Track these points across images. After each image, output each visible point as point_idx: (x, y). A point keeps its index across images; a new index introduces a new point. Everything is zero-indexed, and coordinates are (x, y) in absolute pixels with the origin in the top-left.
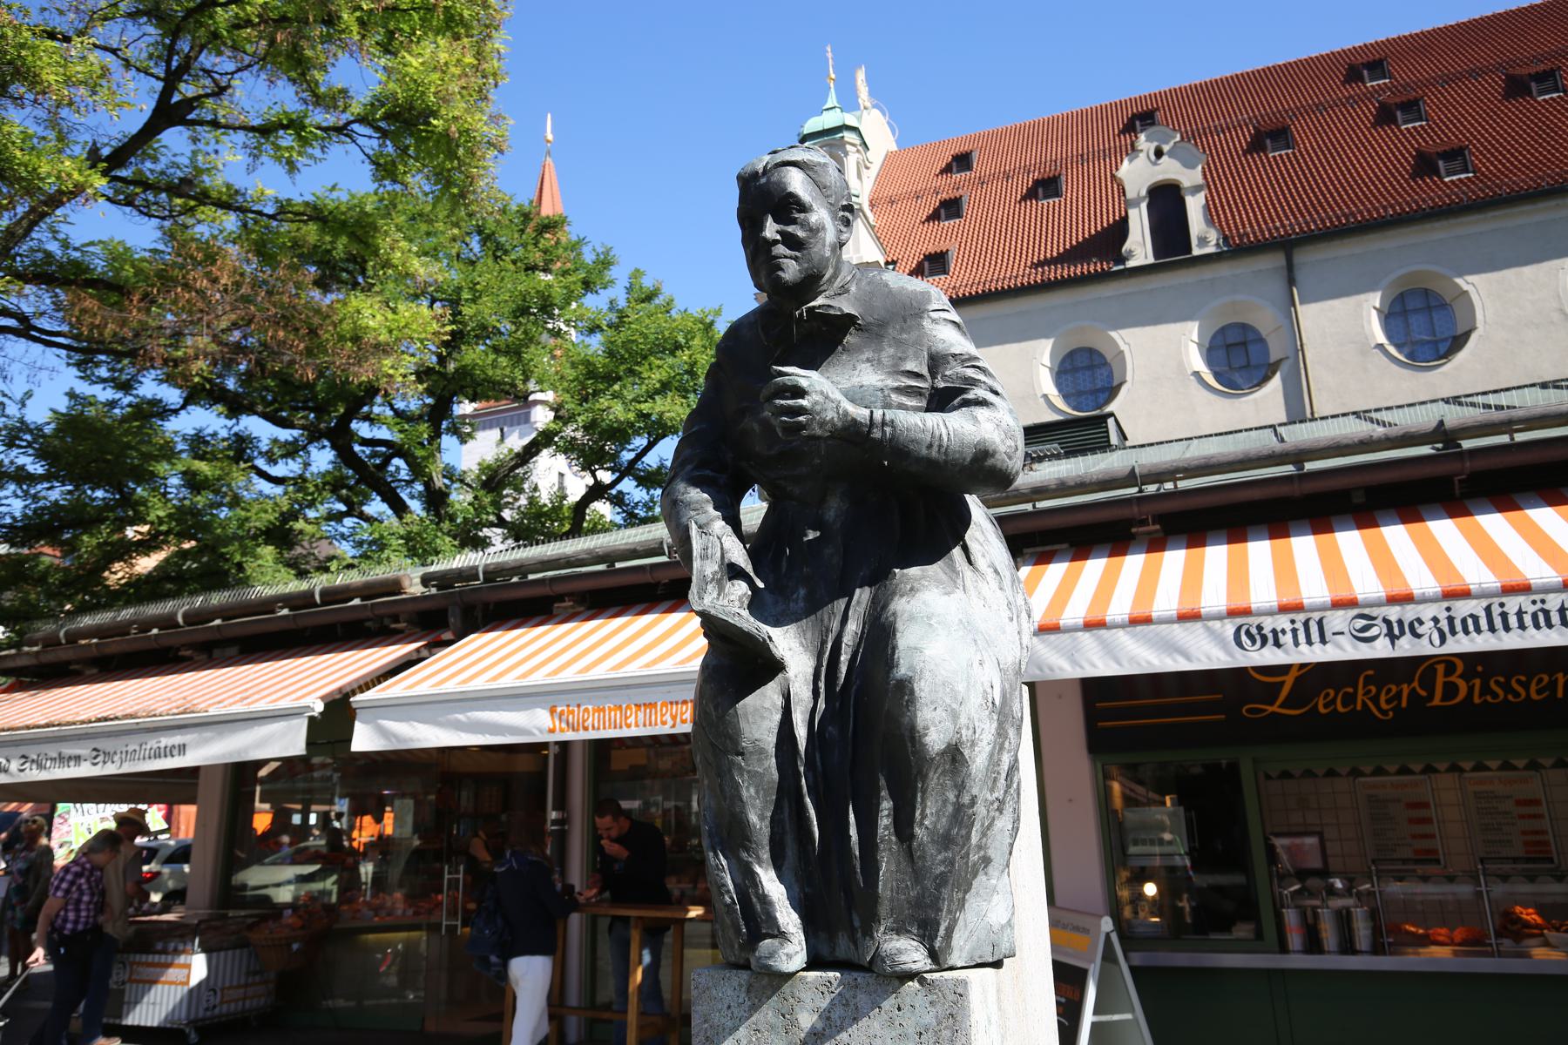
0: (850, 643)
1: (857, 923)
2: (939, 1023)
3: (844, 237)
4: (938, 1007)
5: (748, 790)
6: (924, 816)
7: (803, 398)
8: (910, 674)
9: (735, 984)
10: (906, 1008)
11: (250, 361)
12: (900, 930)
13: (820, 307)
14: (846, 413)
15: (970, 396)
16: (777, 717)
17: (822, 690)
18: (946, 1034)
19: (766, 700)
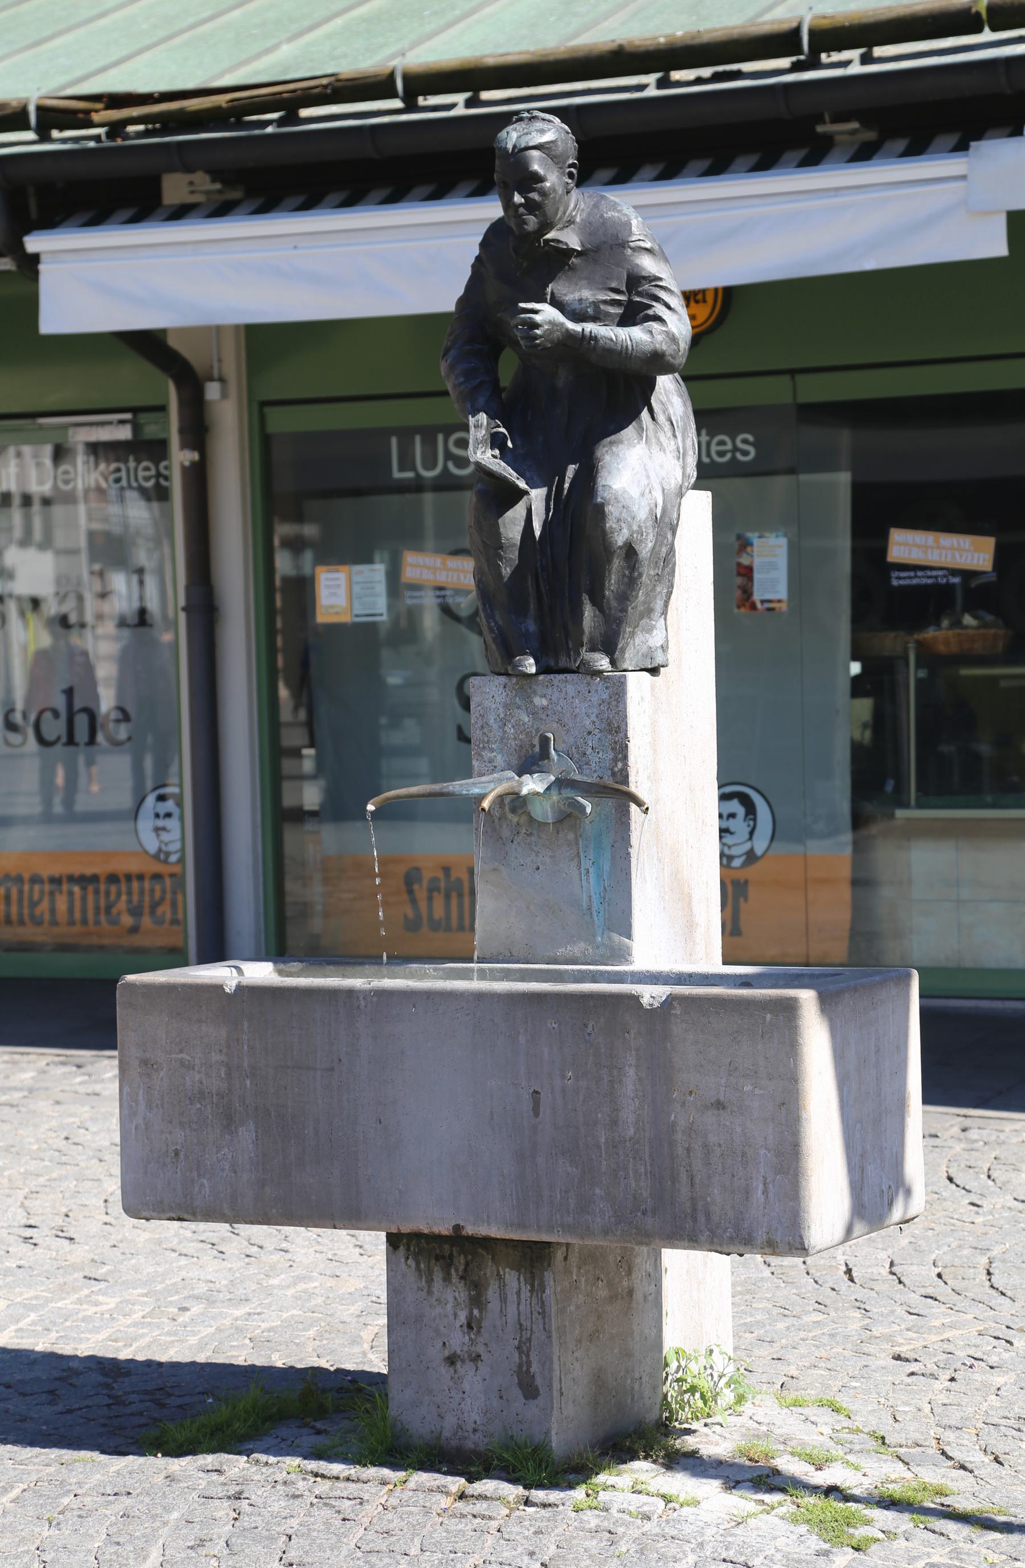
0: (571, 476)
1: (570, 645)
2: (611, 698)
4: (611, 689)
5: (505, 569)
6: (610, 585)
10: (593, 692)
12: (593, 649)
13: (553, 240)
14: (567, 330)
15: (650, 312)
16: (523, 523)
19: (517, 513)
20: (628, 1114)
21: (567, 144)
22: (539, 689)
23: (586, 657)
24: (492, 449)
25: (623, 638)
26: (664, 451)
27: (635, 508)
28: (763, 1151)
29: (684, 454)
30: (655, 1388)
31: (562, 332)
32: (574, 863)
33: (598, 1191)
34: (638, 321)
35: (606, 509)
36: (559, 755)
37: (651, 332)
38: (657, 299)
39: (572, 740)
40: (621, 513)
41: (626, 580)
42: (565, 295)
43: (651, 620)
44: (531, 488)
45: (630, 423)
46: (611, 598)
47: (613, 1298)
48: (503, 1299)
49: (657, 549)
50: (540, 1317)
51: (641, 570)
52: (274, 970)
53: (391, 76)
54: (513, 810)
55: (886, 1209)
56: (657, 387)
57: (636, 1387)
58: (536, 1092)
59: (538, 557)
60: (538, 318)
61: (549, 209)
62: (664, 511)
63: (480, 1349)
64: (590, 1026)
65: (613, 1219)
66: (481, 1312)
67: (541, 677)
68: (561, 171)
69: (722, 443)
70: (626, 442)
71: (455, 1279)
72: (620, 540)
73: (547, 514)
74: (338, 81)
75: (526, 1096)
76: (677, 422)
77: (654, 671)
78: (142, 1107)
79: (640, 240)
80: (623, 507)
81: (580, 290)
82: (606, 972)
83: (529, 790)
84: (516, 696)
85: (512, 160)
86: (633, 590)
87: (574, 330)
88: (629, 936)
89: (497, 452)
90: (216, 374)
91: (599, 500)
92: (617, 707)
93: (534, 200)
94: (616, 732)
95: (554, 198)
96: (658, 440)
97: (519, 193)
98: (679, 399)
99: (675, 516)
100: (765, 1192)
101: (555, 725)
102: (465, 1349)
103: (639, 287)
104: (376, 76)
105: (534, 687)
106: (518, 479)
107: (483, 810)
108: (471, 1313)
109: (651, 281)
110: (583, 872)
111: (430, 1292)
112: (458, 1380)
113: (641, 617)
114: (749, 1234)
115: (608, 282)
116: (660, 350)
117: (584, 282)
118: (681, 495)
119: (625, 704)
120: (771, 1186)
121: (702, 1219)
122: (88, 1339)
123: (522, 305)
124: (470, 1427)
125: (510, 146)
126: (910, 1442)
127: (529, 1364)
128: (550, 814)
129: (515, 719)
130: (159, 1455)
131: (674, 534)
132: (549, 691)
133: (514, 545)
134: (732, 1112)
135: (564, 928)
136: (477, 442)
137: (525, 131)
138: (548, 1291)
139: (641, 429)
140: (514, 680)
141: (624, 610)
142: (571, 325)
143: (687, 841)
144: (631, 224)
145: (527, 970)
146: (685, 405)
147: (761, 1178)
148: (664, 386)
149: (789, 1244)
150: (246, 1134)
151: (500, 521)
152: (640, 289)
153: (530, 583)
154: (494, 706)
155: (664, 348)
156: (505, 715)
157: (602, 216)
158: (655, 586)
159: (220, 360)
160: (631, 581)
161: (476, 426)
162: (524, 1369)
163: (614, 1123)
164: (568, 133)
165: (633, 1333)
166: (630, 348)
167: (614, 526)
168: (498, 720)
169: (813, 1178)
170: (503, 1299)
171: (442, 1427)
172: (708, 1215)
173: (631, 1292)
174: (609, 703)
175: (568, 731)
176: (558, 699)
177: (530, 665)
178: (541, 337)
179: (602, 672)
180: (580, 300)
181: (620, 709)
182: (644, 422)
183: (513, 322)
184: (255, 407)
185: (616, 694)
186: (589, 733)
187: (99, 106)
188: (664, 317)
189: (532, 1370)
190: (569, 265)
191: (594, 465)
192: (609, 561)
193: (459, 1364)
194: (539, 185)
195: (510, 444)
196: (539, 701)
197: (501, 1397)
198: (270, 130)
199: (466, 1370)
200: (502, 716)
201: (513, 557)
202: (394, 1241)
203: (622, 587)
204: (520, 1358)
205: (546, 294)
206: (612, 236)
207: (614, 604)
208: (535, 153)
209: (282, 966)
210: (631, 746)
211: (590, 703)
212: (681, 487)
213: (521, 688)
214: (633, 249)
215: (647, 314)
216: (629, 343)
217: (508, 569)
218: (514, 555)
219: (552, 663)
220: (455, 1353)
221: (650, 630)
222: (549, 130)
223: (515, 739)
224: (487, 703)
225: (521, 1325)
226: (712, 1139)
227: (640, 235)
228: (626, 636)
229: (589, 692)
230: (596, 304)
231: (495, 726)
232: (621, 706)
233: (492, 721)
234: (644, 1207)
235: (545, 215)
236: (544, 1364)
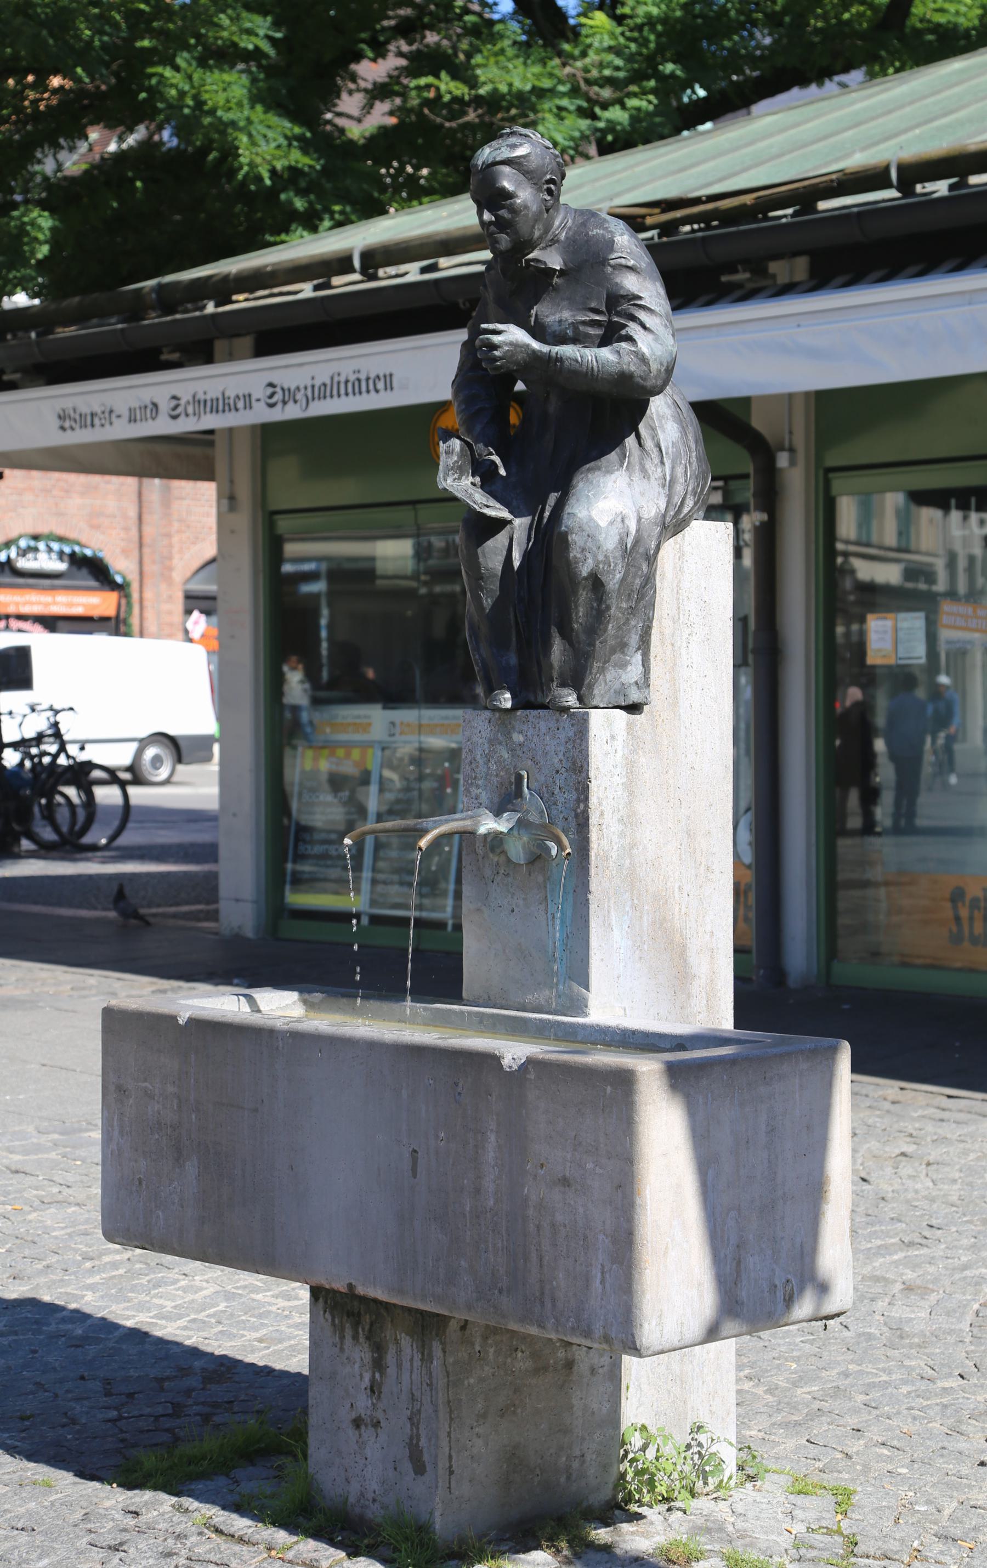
0: (552, 504)
1: (543, 680)
11: (49, 814)
12: (563, 685)
15: (623, 332)
16: (505, 553)
18: (578, 741)
19: (500, 540)
20: (489, 1184)
21: (543, 159)
22: (517, 725)
24: (473, 476)
25: (591, 673)
26: (649, 479)
27: (601, 538)
28: (601, 1237)
30: (605, 1467)
32: (542, 907)
33: (463, 1263)
35: (570, 538)
36: (531, 794)
37: (618, 352)
38: (633, 318)
39: (543, 779)
41: (594, 612)
42: (547, 316)
43: (626, 655)
47: (540, 1370)
48: (399, 1366)
49: (629, 579)
50: (428, 1389)
51: (608, 602)
52: (299, 1000)
53: (887, 169)
54: (492, 850)
55: (781, 1305)
57: (576, 1465)
58: (415, 1151)
60: (496, 339)
62: (637, 542)
63: (380, 1415)
64: (460, 1085)
65: (474, 1294)
66: (381, 1377)
67: (519, 713)
71: (362, 1339)
72: (585, 571)
73: (528, 544)
74: (845, 174)
75: (407, 1155)
76: (667, 448)
77: (634, 708)
78: (116, 1133)
79: (620, 257)
82: (564, 1023)
83: (488, 830)
87: (541, 352)
88: (587, 988)
89: (478, 479)
90: (787, 445)
91: (563, 528)
94: (580, 772)
95: (526, 215)
96: (643, 467)
97: (489, 211)
98: (675, 425)
100: (603, 1282)
101: (529, 762)
102: (369, 1413)
104: (875, 168)
105: (513, 722)
107: (420, 849)
108: (373, 1376)
109: (630, 300)
110: (550, 917)
111: (342, 1350)
112: (361, 1445)
113: (613, 651)
114: (589, 1326)
117: (565, 303)
119: (587, 742)
120: (607, 1276)
121: (548, 1305)
122: (243, 1336)
123: (484, 326)
124: (370, 1496)
126: (879, 1552)
127: (418, 1436)
128: (522, 855)
130: (115, 1485)
132: (525, 728)
133: (496, 575)
134: (576, 1190)
135: (532, 975)
136: (448, 469)
138: (435, 1362)
140: (497, 715)
143: (680, 888)
145: (498, 1015)
147: (600, 1266)
148: (657, 411)
149: (622, 1341)
150: (191, 1168)
151: (479, 550)
152: (619, 309)
154: (480, 741)
155: (633, 368)
158: (628, 619)
159: (791, 433)
160: (599, 615)
161: (449, 453)
162: (414, 1442)
163: (478, 1191)
164: (548, 148)
165: (572, 1408)
166: (596, 369)
167: (578, 556)
169: (648, 1271)
170: (399, 1366)
171: (348, 1492)
172: (554, 1301)
173: (570, 1365)
175: (540, 769)
177: (506, 700)
178: (501, 358)
180: (560, 321)
184: (821, 473)
186: (557, 772)
187: (657, 210)
188: (635, 337)
189: (421, 1444)
192: (575, 593)
193: (363, 1427)
194: (508, 202)
195: (502, 472)
196: (518, 738)
197: (395, 1469)
198: (784, 220)
199: (368, 1433)
200: (487, 752)
202: (316, 1293)
204: (412, 1430)
205: (530, 316)
207: (583, 637)
208: (506, 169)
209: (306, 996)
210: (593, 786)
212: (664, 516)
214: (614, 267)
216: (595, 363)
218: (495, 586)
219: (532, 699)
220: (360, 1416)
221: (623, 665)
222: (521, 145)
223: (497, 775)
224: (475, 739)
225: (413, 1395)
226: (559, 1218)
228: (594, 671)
230: (575, 325)
231: (481, 762)
232: (584, 744)
233: (479, 757)
234: (499, 1285)
236: (430, 1440)
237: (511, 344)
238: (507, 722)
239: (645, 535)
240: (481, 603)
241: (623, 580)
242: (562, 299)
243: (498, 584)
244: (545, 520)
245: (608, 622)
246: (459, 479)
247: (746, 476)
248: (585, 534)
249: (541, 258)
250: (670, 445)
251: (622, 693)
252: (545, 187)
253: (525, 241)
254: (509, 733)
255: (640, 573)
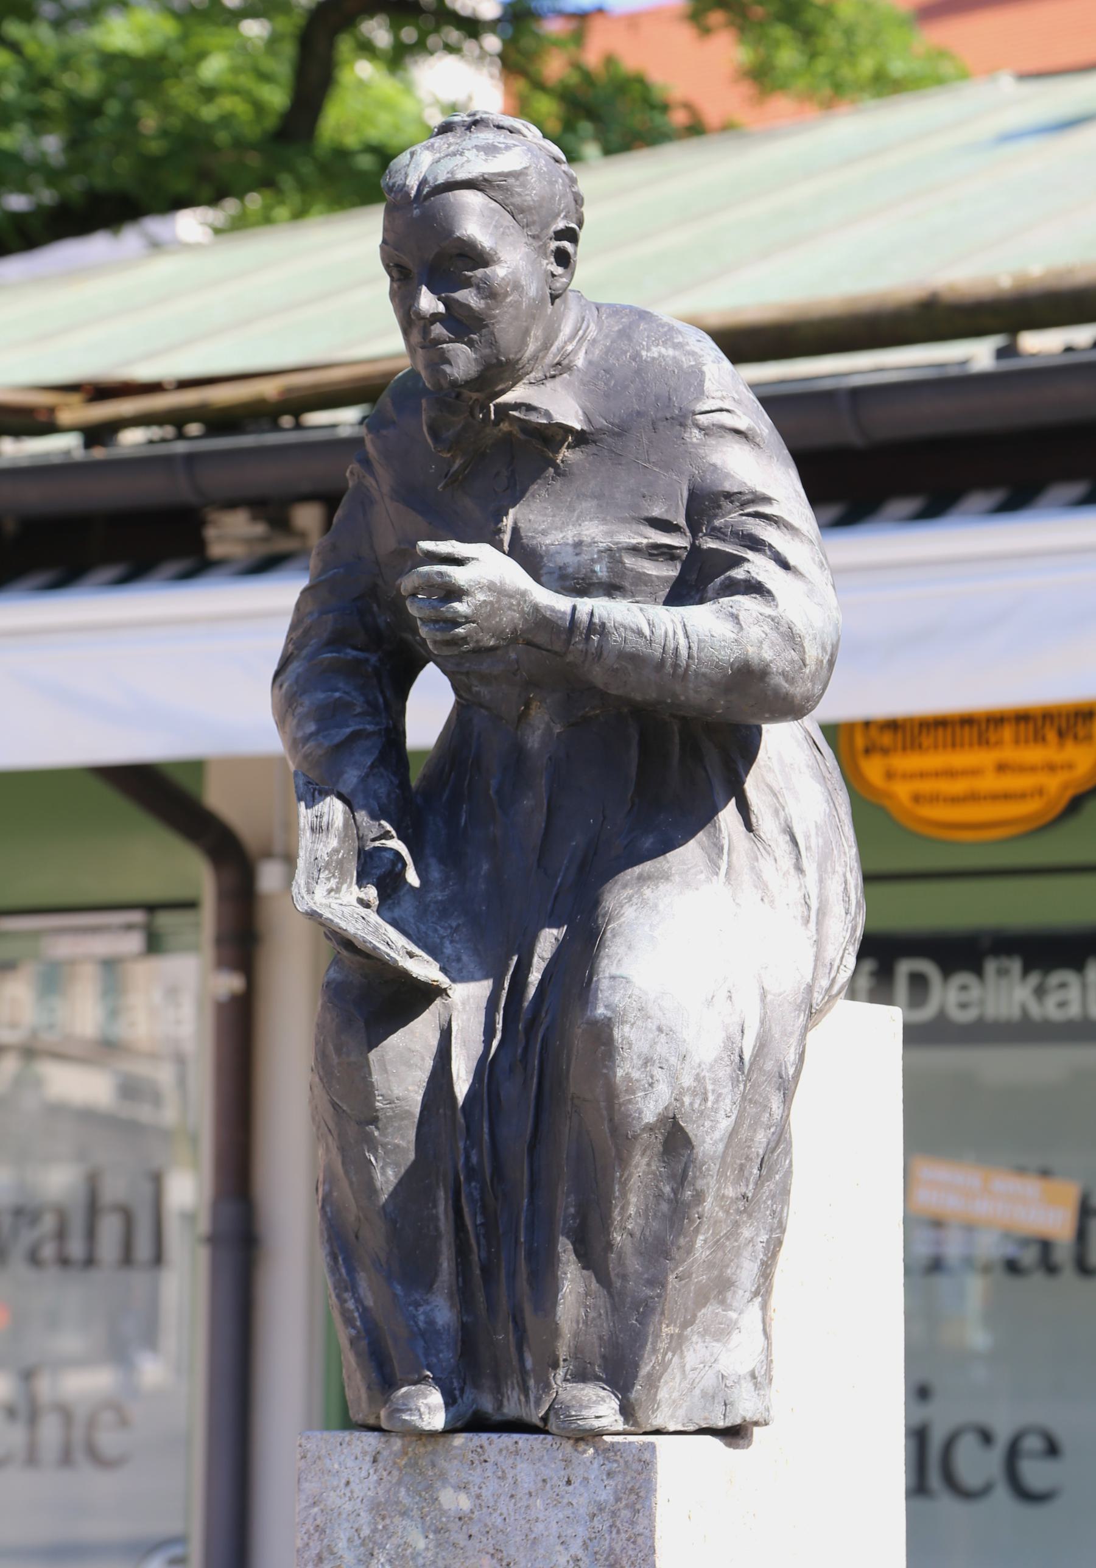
0: (548, 955)
1: (529, 1364)
2: (618, 1500)
3: (558, 284)
4: (619, 1478)
5: (383, 1173)
7: (460, 601)
8: (609, 1014)
9: (358, 1451)
10: (576, 1482)
12: (581, 1376)
13: (517, 406)
14: (536, 608)
15: (738, 573)
16: (429, 1064)
17: (499, 1026)
21: (552, 183)
22: (453, 1469)
23: (564, 1396)
24: (360, 883)
25: (654, 1351)
29: (822, 912)
31: (522, 612)
34: (710, 594)
35: (617, 1034)
37: (735, 618)
38: (756, 544)
40: (654, 1043)
41: (664, 1207)
42: (544, 533)
44: (453, 980)
45: (693, 834)
46: (629, 1249)
49: (743, 1133)
51: (700, 1184)
56: (761, 755)
59: (461, 1145)
60: (458, 575)
61: (505, 329)
62: (762, 1045)
67: (459, 1440)
68: (536, 244)
69: (963, 1006)
70: (677, 878)
73: (487, 1043)
76: (807, 837)
79: (721, 410)
80: (660, 1030)
81: (578, 522)
84: (399, 1483)
85: (416, 212)
86: (680, 1232)
87: (553, 610)
89: (371, 893)
91: (601, 1011)
92: (633, 1523)
93: (468, 307)
95: (516, 305)
96: (759, 877)
99: (792, 1056)
103: (715, 516)
105: (442, 1463)
106: (411, 955)
109: (744, 504)
113: (702, 1299)
115: (644, 503)
116: (755, 661)
117: (588, 505)
118: (813, 1014)
119: (651, 1517)
125: (413, 182)
129: (395, 1540)
131: (787, 1098)
132: (475, 1476)
133: (409, 1114)
136: (317, 867)
137: (452, 148)
139: (717, 849)
140: (397, 1444)
141: (658, 1282)
142: (560, 603)
144: (702, 373)
146: (831, 800)
151: (373, 1055)
152: (717, 523)
153: (441, 1208)
154: (348, 1507)
155: (768, 654)
156: (374, 1531)
157: (636, 356)
158: (736, 1224)
161: (317, 829)
166: (684, 652)
167: (636, 1075)
168: (357, 1542)
174: (614, 1514)
176: (497, 1496)
178: (468, 620)
179: (599, 1434)
180: (578, 545)
181: (639, 1529)
182: (725, 833)
183: (407, 584)
185: (632, 1490)
188: (769, 585)
190: (556, 467)
191: (598, 928)
192: (623, 1161)
194: (479, 273)
195: (412, 877)
200: (366, 1532)
201: (403, 1143)
203: (655, 1225)
206: (657, 400)
207: (634, 1264)
208: (472, 198)
211: (568, 1511)
212: (810, 989)
213: (413, 1464)
215: (729, 577)
216: (683, 642)
217: (390, 1172)
219: (487, 1404)
221: (722, 1332)
222: (508, 148)
224: (333, 1499)
227: (722, 398)
228: (662, 1345)
229: (569, 1482)
230: (613, 555)
231: (349, 1558)
232: (642, 1521)
233: (342, 1545)
235: (493, 343)
237: (491, 587)
238: (423, 1462)
239: (776, 1032)
240: (370, 1181)
241: (734, 1132)
242: (581, 496)
243: (412, 1134)
244: (531, 991)
245: (697, 1231)
246: (337, 890)
247: (190, 905)
248: (652, 1025)
249: (535, 403)
250: (813, 832)
251: (720, 1399)
252: (554, 245)
253: (508, 361)
254: (429, 1488)
255: (765, 1117)
